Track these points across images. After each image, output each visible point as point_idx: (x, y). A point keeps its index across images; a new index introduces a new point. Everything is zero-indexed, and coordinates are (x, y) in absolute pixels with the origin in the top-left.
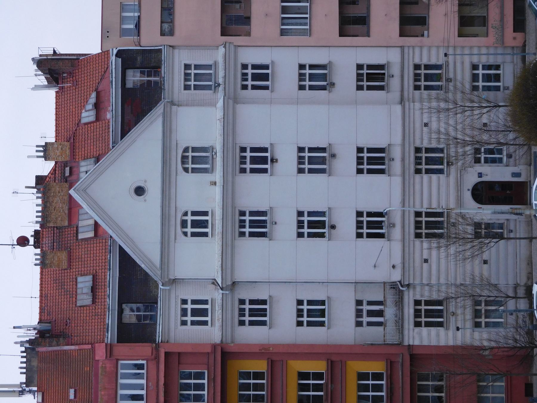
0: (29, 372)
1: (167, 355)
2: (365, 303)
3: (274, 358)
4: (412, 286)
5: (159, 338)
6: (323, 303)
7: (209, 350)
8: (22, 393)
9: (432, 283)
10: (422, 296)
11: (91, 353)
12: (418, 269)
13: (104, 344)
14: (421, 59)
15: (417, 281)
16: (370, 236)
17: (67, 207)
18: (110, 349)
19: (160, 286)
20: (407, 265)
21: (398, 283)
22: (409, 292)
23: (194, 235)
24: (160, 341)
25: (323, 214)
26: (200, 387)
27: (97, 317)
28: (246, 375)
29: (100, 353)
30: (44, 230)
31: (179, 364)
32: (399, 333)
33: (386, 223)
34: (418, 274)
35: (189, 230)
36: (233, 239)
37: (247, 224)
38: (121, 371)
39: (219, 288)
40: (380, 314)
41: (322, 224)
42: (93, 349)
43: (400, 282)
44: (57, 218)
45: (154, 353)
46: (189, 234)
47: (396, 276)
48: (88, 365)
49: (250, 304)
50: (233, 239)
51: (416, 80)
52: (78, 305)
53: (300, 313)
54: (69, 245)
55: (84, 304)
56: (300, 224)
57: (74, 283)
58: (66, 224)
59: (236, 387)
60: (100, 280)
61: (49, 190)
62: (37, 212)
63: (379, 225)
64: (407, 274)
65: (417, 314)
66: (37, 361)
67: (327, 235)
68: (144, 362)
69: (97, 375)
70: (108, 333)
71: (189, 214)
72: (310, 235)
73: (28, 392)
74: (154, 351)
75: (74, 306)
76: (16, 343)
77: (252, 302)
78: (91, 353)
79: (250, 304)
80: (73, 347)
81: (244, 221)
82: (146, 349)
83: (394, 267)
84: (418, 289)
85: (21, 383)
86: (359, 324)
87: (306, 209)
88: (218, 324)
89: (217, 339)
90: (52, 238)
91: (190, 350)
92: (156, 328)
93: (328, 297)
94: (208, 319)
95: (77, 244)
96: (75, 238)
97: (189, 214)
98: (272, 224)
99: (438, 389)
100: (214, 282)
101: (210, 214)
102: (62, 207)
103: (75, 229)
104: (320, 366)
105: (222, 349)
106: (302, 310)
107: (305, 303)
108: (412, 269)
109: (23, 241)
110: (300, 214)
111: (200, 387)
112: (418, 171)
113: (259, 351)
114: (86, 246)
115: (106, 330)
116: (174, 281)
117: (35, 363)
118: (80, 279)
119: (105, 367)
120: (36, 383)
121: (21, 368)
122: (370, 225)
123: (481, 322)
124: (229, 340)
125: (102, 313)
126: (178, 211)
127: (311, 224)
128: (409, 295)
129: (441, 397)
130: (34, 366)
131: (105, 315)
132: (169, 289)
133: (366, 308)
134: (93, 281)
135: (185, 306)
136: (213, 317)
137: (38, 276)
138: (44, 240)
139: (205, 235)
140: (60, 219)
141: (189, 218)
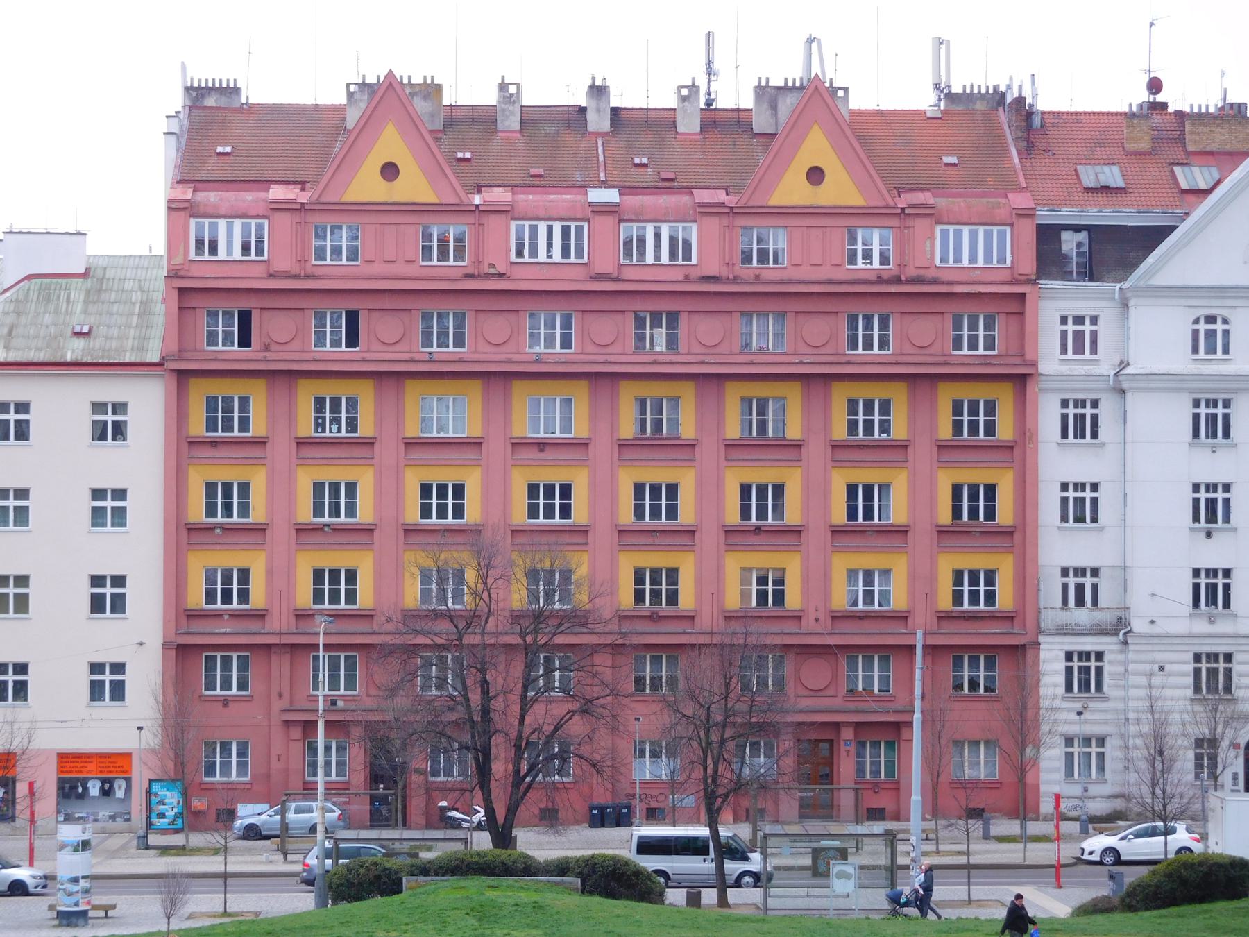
0: (966, 98)
1: (1023, 296)
2: (1095, 580)
3: (1016, 451)
4: (1124, 647)
5: (1044, 284)
6: (1095, 520)
7: (1029, 356)
8: (937, 87)
9: (1130, 677)
10: (1110, 662)
11: (1014, 187)
12: (1149, 657)
13: (1034, 206)
14: (1239, 663)
15: (1131, 656)
16: (1196, 587)
17: (1214, 149)
18: (1028, 214)
19: (1118, 286)
20: (1156, 641)
21: (1129, 628)
22: (1116, 644)
23: (1195, 333)
24: (1040, 286)
25: (1227, 519)
26: (973, 345)
27: (1066, 194)
28: (990, 410)
29: (1020, 200)
30: (1173, 117)
31: (796, 312)
32: (1057, 629)
33: (1215, 611)
34: (1143, 657)
35: (1202, 327)
36: (1191, 391)
37: (1212, 411)
38: (995, 229)
39: (1117, 370)
40: (1080, 602)
41: (1212, 518)
42: (1020, 190)
43: (1130, 631)
44: (1198, 134)
45: (1023, 278)
46: (1196, 327)
47: (1139, 626)
48: (996, 183)
49: (1092, 415)
50: (1191, 391)
51: (1208, 655)
52: (1078, 167)
53: (1080, 486)
54: (1160, 153)
55: (1081, 177)
56: (1211, 487)
57: (1107, 162)
58: (1190, 148)
59: (974, 396)
60: (1120, 199)
61: (1240, 123)
62: (1207, 107)
63: (1212, 601)
64: (1143, 641)
65: (1085, 656)
66: (983, 109)
67: (1197, 525)
68: (1008, 264)
69: (983, 195)
70: (1048, 211)
71: (1226, 327)
72: (1196, 502)
73: (940, 96)
74: (1025, 277)
75: (1075, 161)
76: (1011, 79)
77: (1095, 419)
78: (1014, 187)
79: (1092, 415)
80: (1016, 160)
81: (1215, 406)
82: (1028, 266)
83: (1152, 622)
84: (1121, 657)
85: (950, 87)
86: (1065, 572)
87: (1233, 495)
88: (1065, 369)
89: (1043, 368)
90: (1164, 128)
91: (1029, 328)
92: (1056, 280)
93: (1102, 528)
94: (1070, 355)
95: (1164, 165)
96: (1172, 161)
97: (1226, 327)
98: (1212, 447)
99: (974, 685)
100: (1124, 364)
101: (1226, 357)
102: (1214, 142)
103: (1185, 161)
104: (1005, 514)
105: (1030, 375)
106: (1083, 490)
107: (1227, 495)
108: (1150, 648)
109: (1155, 85)
110: (1227, 487)
111: (973, 345)
112: (1197, 657)
113: (1028, 427)
114: (1164, 178)
115: (1051, 207)
116: (1125, 306)
117: (980, 106)
118: (1115, 169)
119: (1000, 208)
120: (953, 107)
121: (972, 86)
122: (1212, 588)
123: (1073, 746)
124: (1043, 385)
125: (1073, 203)
126: (1231, 310)
127: (1211, 503)
128: (1111, 643)
129: (962, 689)
130: (975, 104)
131: (1072, 206)
132: (1114, 298)
133: (1088, 581)
134: (1117, 188)
135: (1088, 321)
136: (1073, 363)
137: (1119, 110)
138: (1159, 117)
139: (1195, 350)
140: (1197, 139)
141: (1219, 327)
